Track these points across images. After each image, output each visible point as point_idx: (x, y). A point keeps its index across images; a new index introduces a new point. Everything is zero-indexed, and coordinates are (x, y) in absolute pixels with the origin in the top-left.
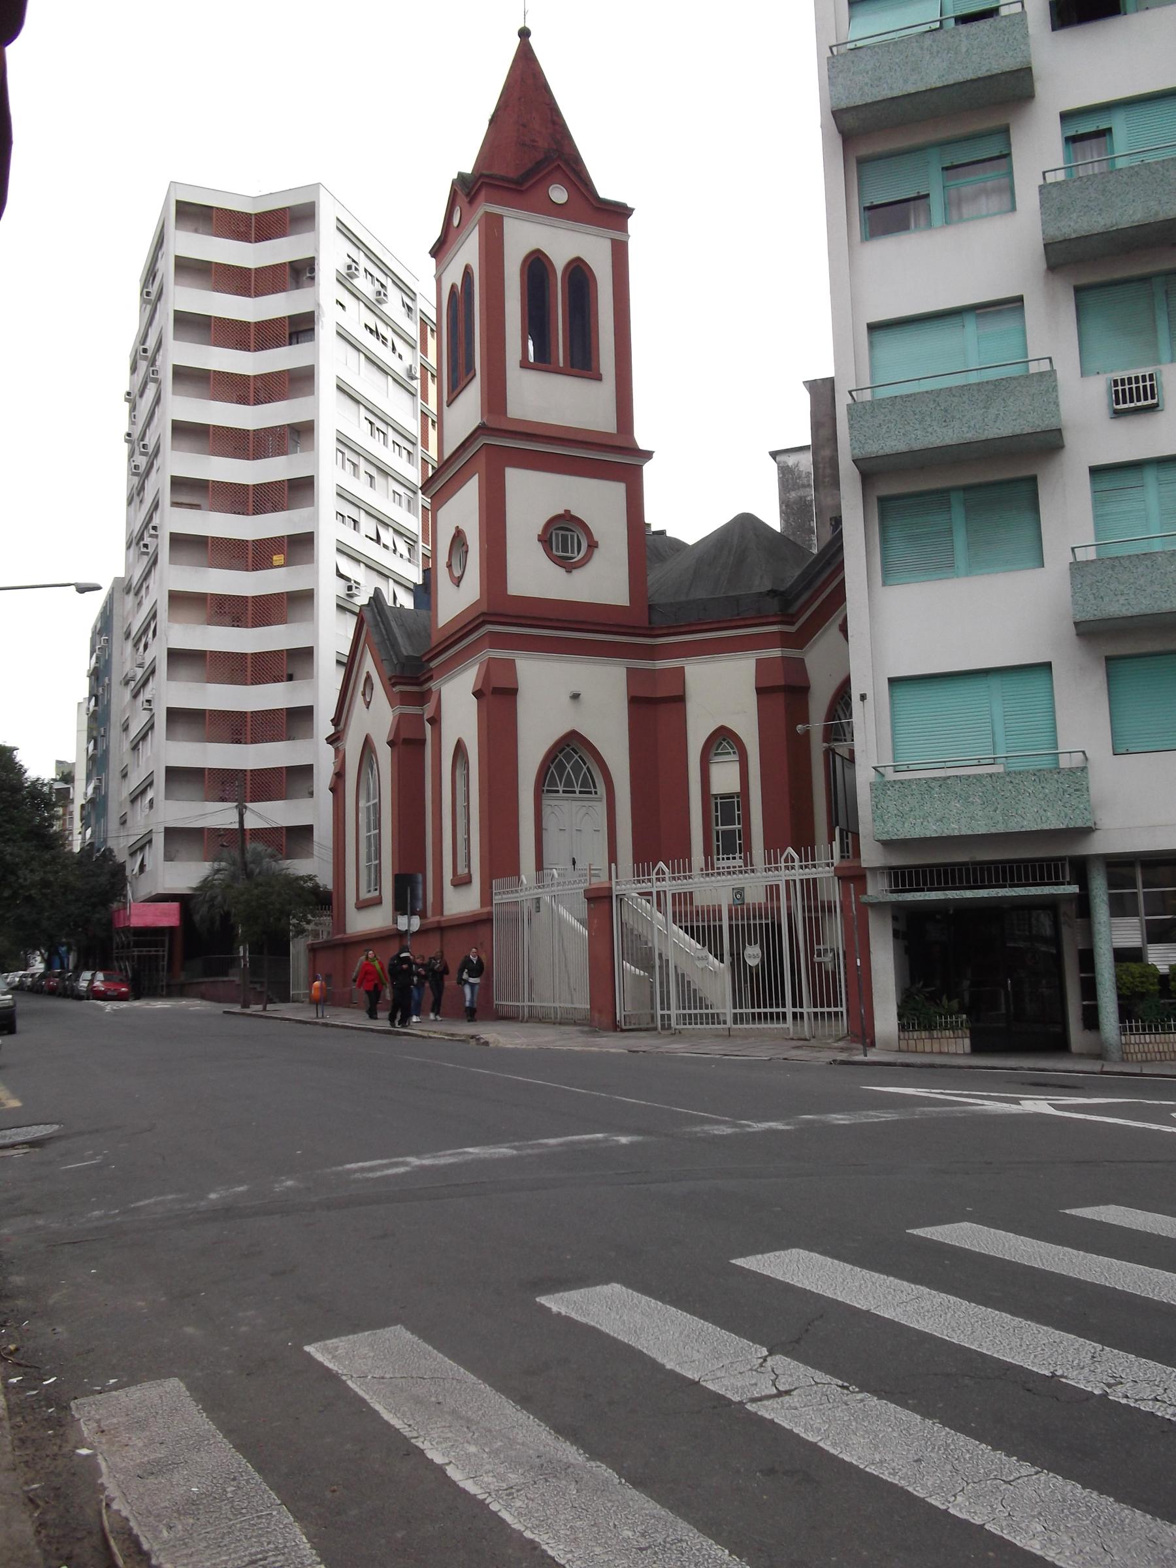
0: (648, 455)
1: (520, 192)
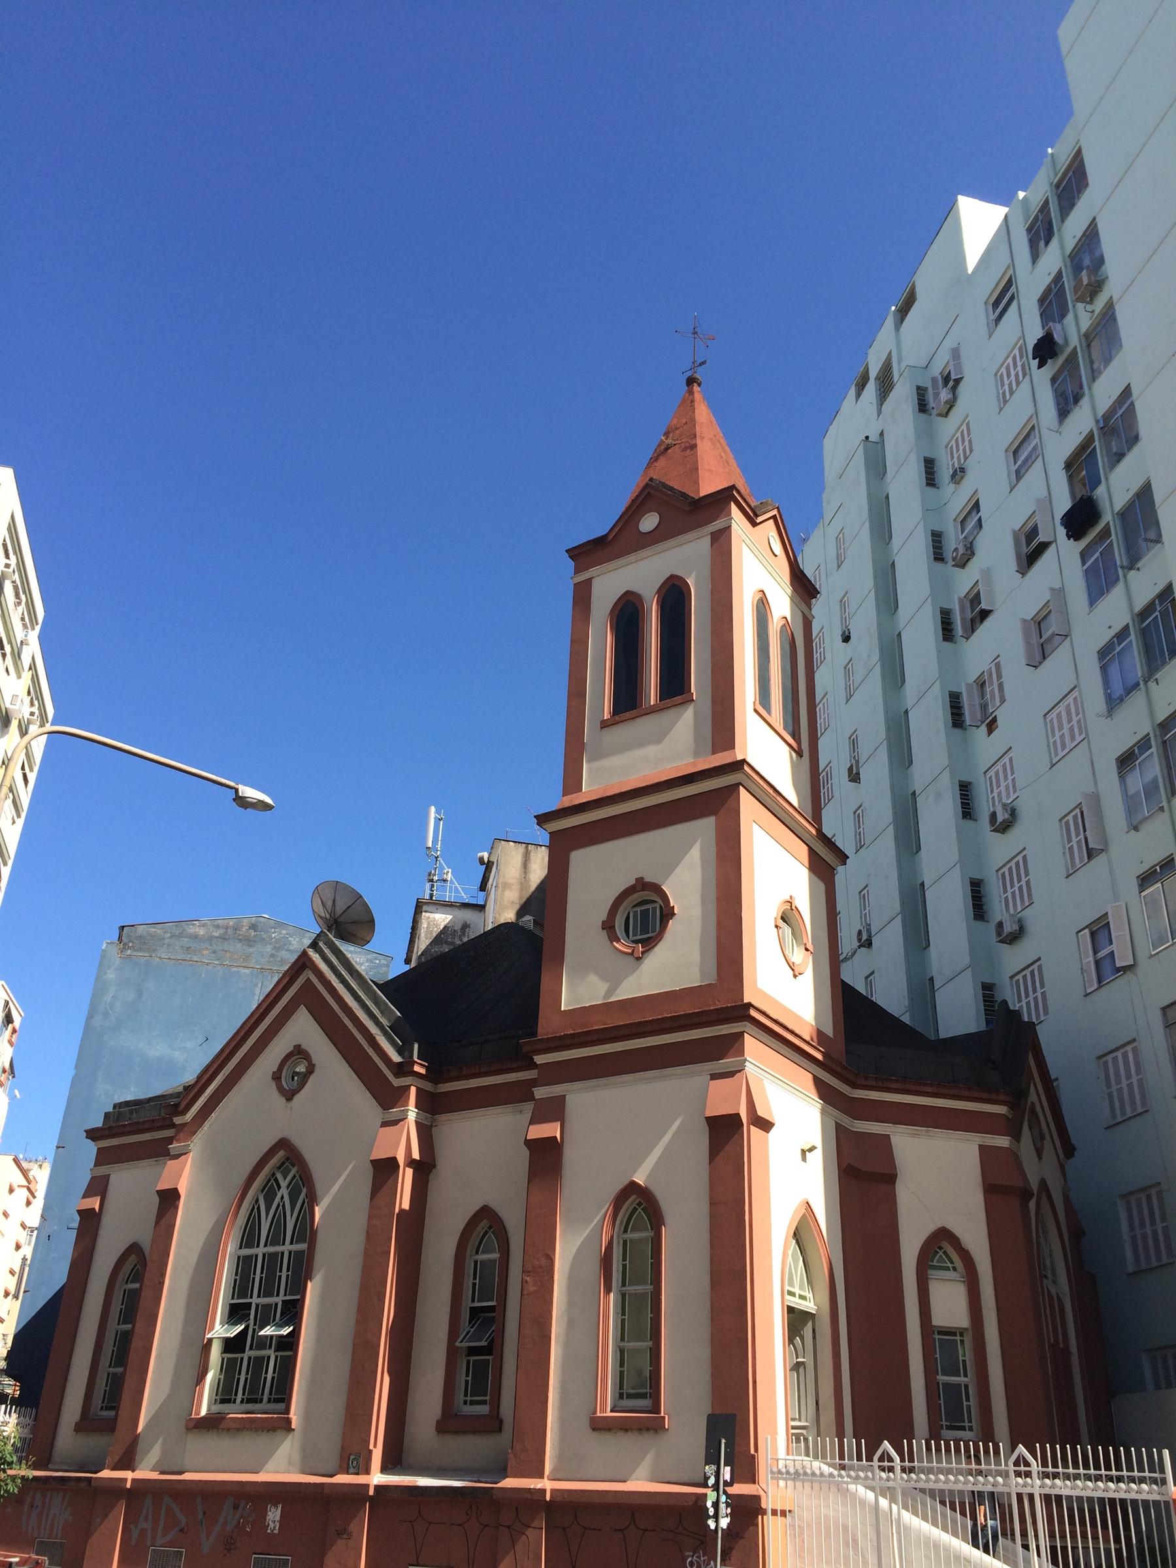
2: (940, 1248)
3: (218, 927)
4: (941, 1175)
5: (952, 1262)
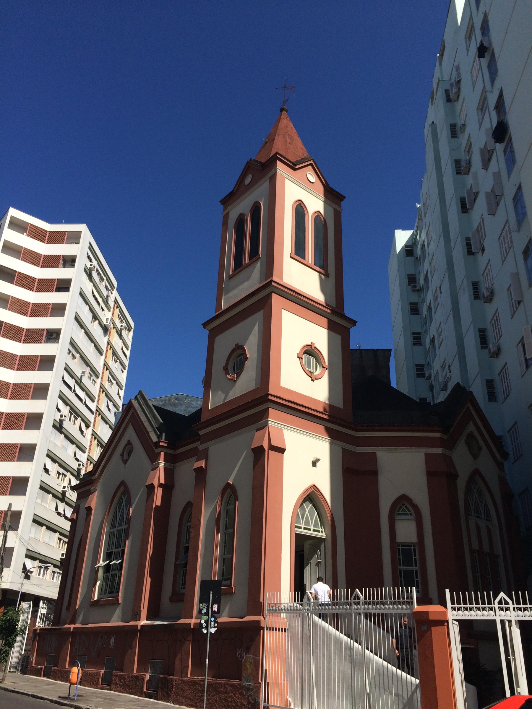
0: (354, 323)
1: (295, 170)
2: (403, 505)
3: (162, 400)
4: (402, 470)
5: (410, 511)
